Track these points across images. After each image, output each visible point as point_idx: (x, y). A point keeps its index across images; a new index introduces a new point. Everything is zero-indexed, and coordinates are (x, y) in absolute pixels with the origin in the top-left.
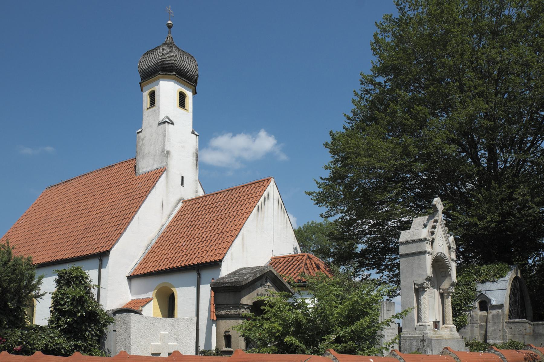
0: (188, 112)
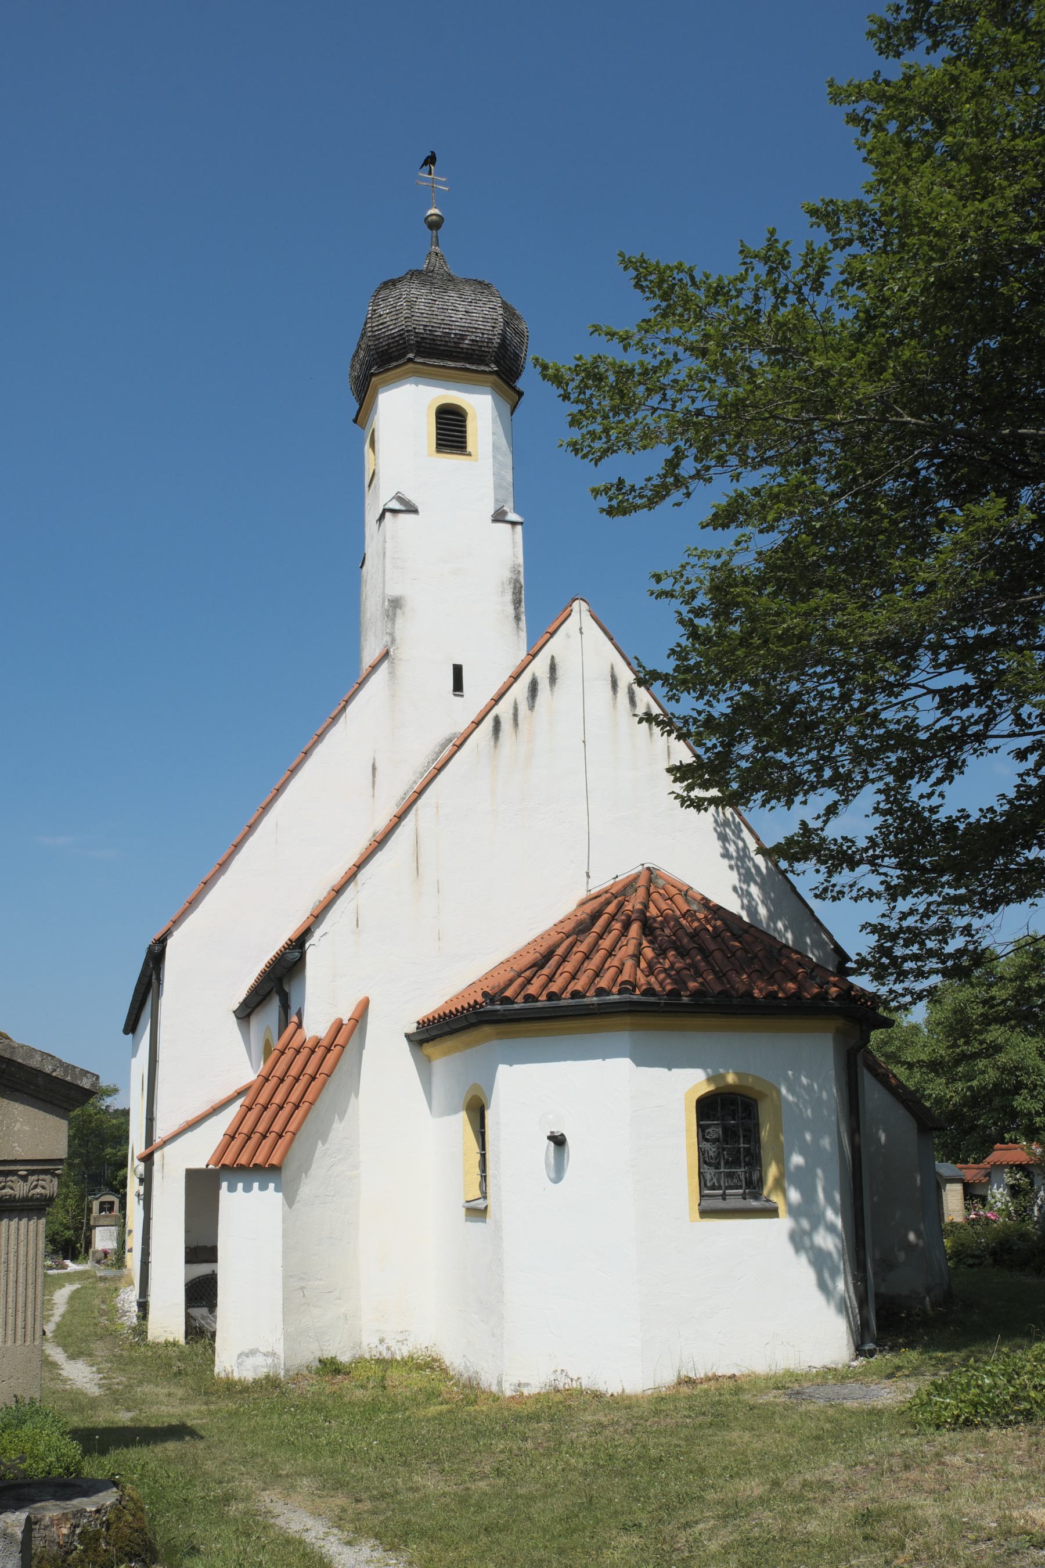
0: (476, 460)
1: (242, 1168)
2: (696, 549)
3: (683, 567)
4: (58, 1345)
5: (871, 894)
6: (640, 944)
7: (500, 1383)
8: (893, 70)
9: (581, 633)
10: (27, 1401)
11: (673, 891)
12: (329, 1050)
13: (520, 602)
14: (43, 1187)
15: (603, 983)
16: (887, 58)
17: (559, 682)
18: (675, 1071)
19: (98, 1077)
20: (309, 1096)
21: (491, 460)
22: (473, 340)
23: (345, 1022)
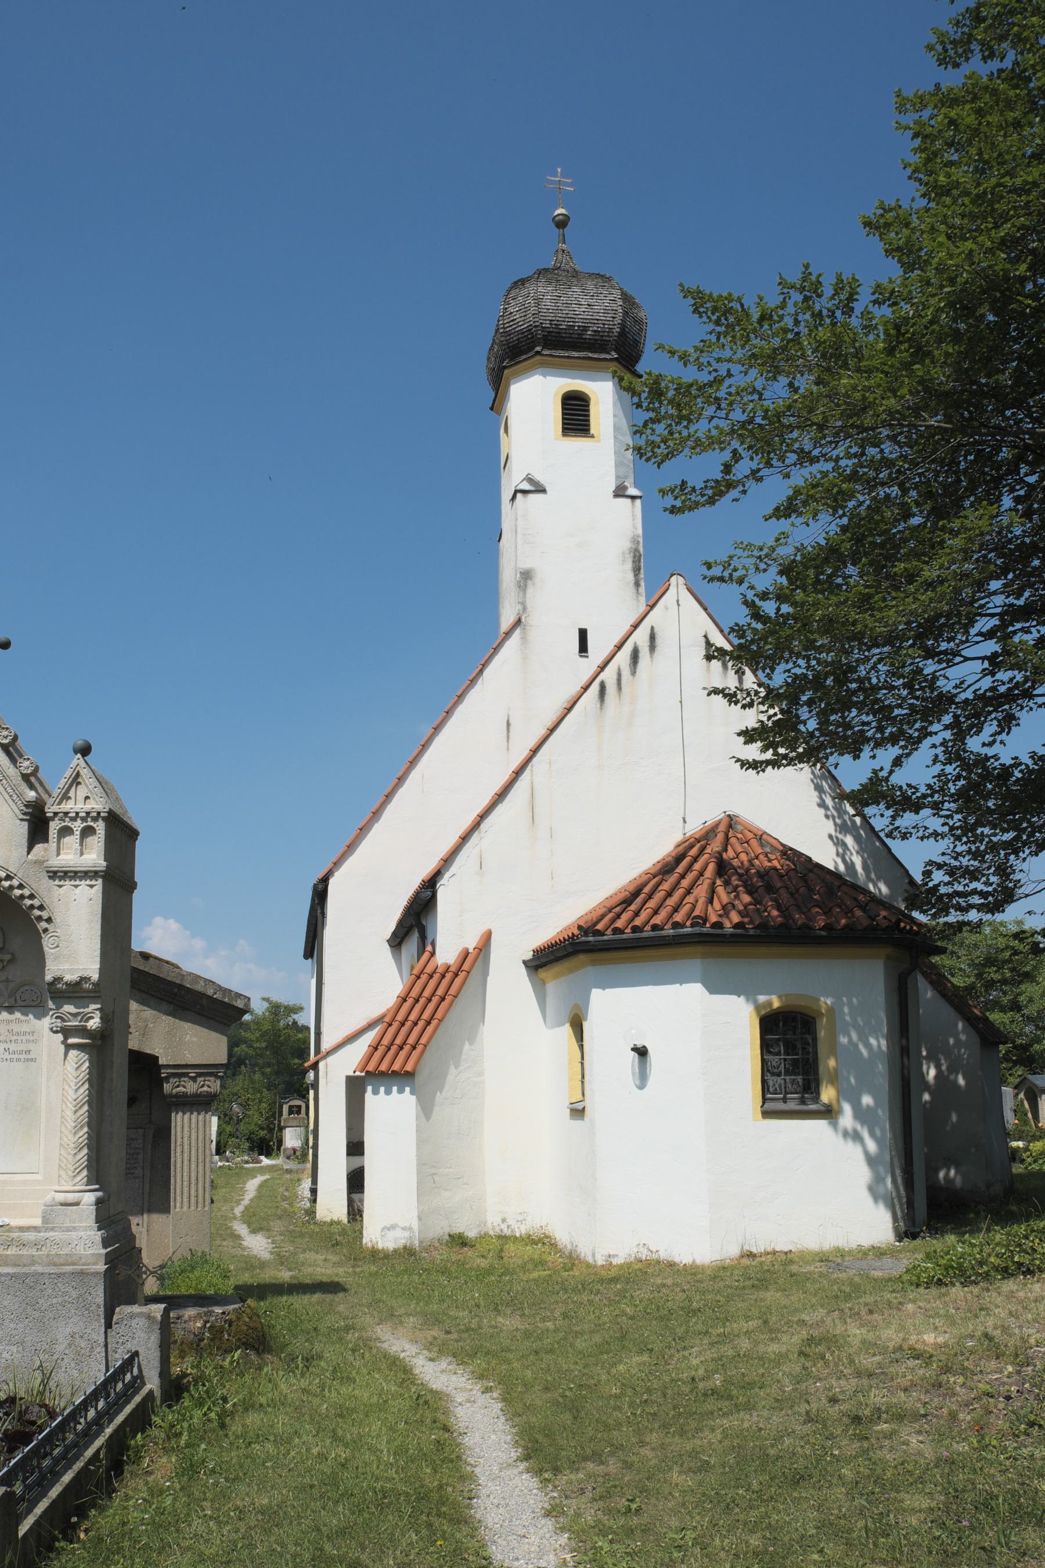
0: (599, 441)
1: (383, 1074)
2: (742, 543)
3: (731, 557)
4: (244, 1223)
5: (936, 835)
6: (714, 883)
7: (594, 1255)
8: (953, 79)
9: (679, 605)
10: (199, 1254)
11: (750, 835)
12: (456, 975)
13: (639, 569)
14: (209, 1086)
15: (678, 917)
16: (946, 68)
17: (658, 649)
18: (608, 990)
19: (249, 999)
20: (438, 1015)
21: (612, 441)
22: (595, 331)
23: (471, 950)
